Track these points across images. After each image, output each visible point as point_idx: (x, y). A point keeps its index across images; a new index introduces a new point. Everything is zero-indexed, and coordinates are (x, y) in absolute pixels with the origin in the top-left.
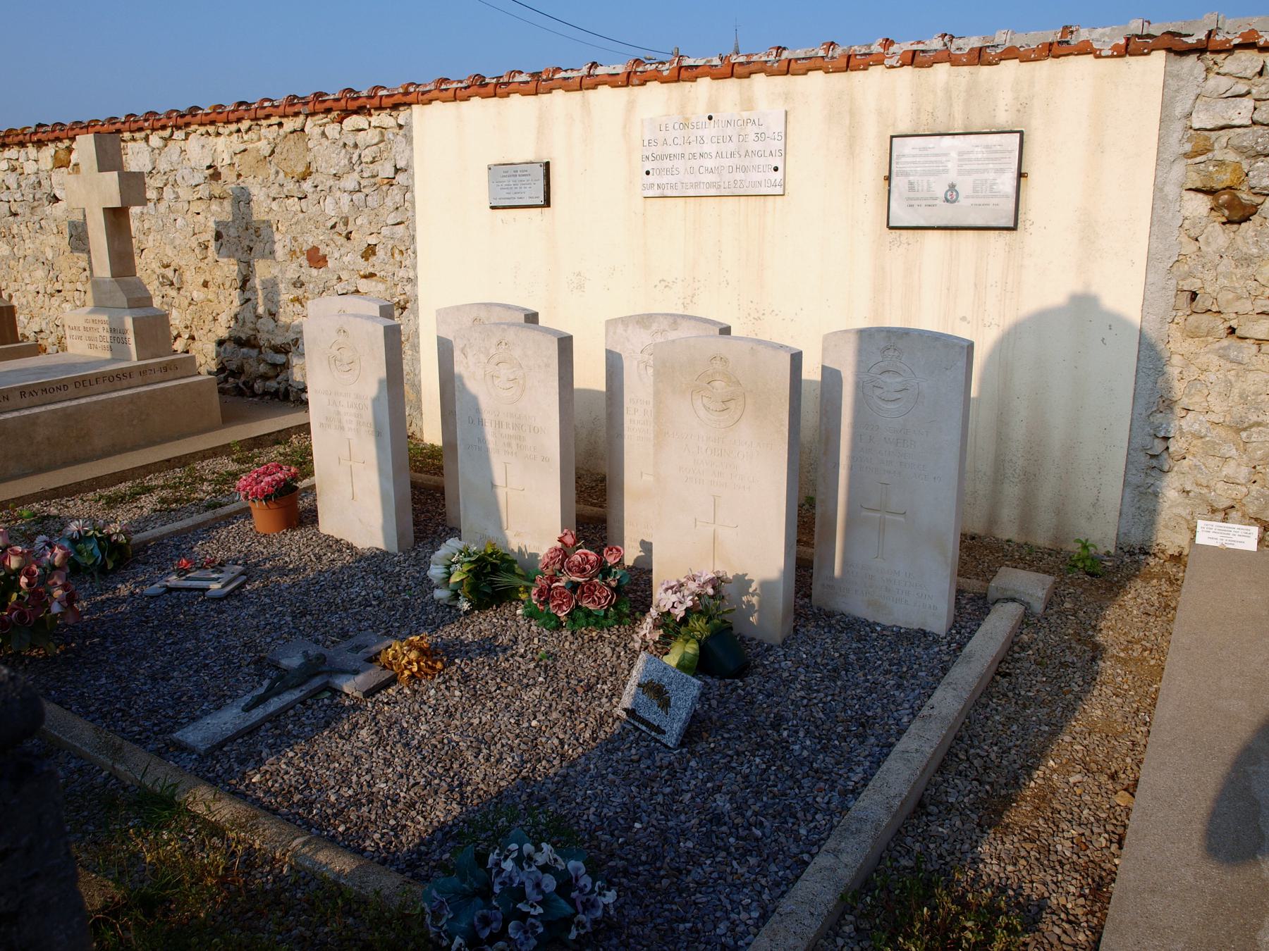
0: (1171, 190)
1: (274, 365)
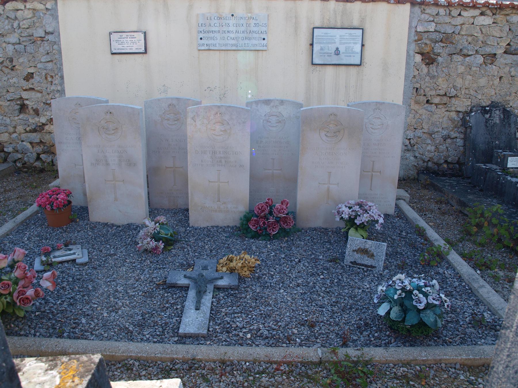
0: (412, 53)
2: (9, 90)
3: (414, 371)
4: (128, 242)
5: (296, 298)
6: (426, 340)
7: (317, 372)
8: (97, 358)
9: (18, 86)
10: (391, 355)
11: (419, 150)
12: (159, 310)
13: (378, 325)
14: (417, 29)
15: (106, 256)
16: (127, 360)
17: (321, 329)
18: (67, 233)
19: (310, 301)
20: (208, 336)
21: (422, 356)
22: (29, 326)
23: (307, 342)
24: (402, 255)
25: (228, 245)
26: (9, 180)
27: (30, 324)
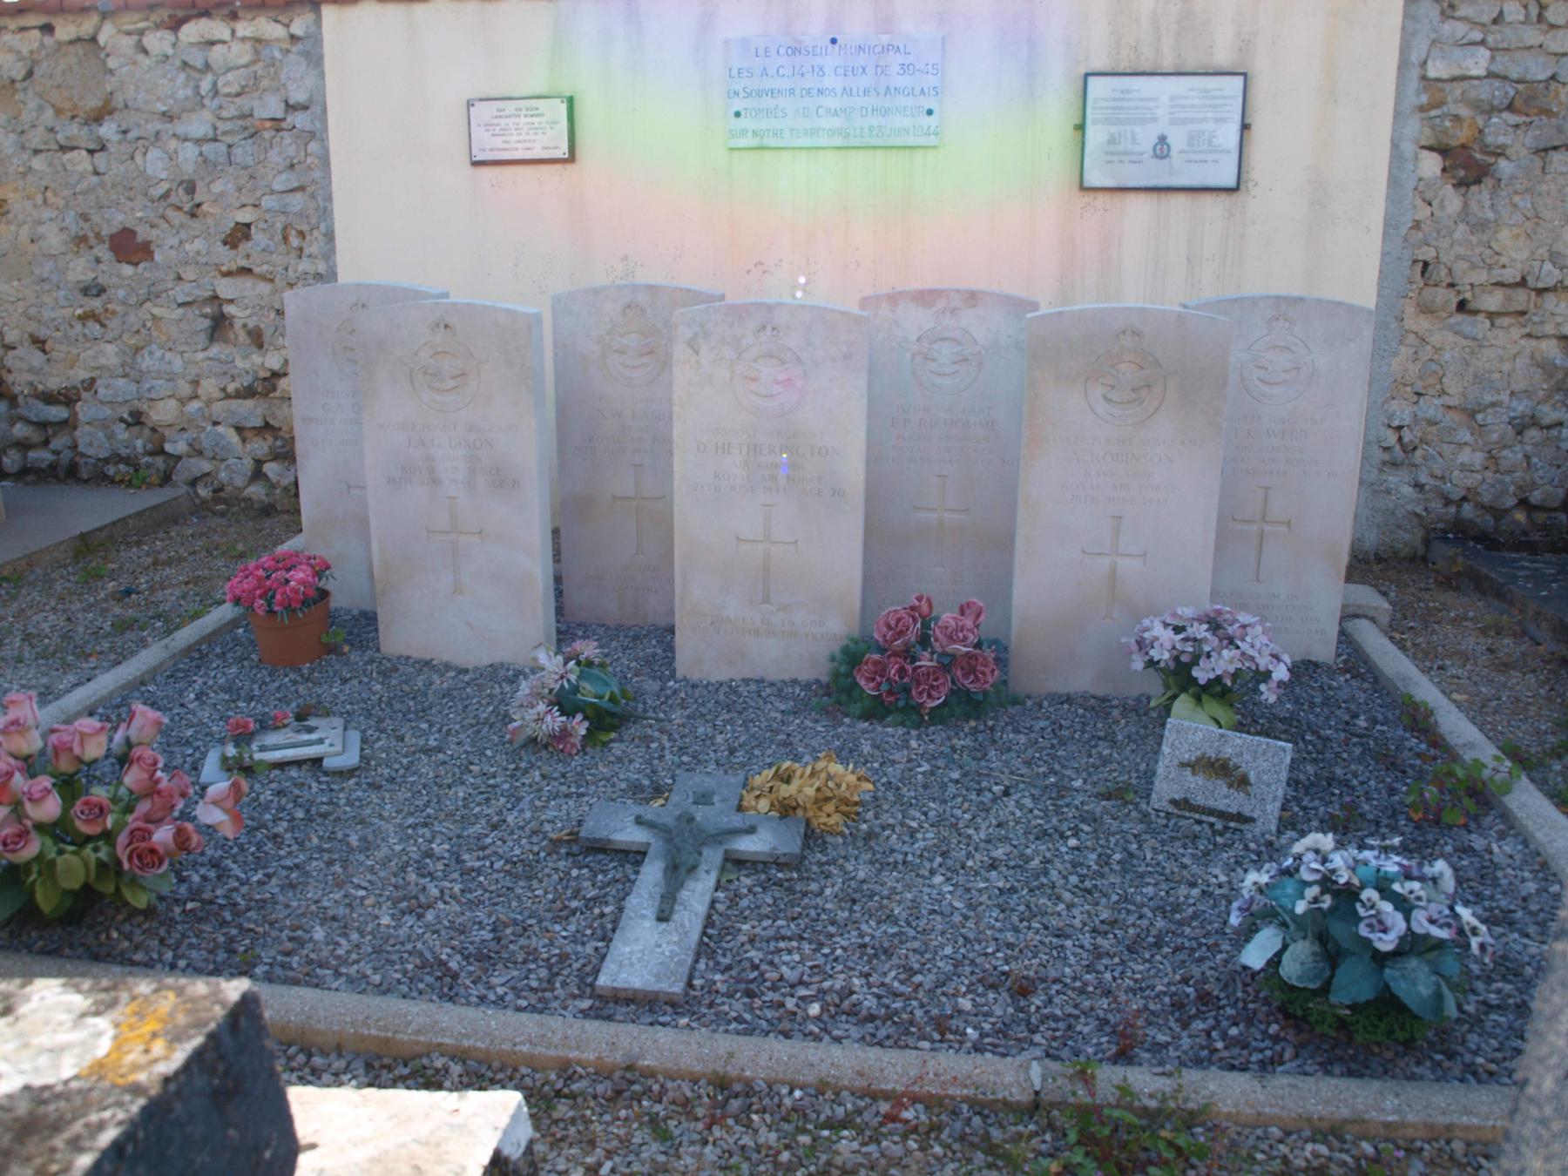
0: (1408, 148)
1: (42, 425)
2: (183, 276)
3: (1352, 1156)
4: (485, 715)
5: (981, 904)
6: (1406, 1059)
7: (1020, 1135)
8: (236, 989)
9: (207, 264)
10: (1275, 1097)
11: (1430, 463)
12: (549, 915)
13: (1244, 1001)
14: (1426, 70)
15: (414, 753)
16: (428, 1055)
17: (1050, 1001)
18: (310, 685)
19: (1027, 914)
20: (687, 1002)
21: (1383, 1110)
22: (162, 940)
23: (1001, 1041)
24: (1348, 786)
25: (788, 735)
26: (172, 534)
27: (162, 932)
